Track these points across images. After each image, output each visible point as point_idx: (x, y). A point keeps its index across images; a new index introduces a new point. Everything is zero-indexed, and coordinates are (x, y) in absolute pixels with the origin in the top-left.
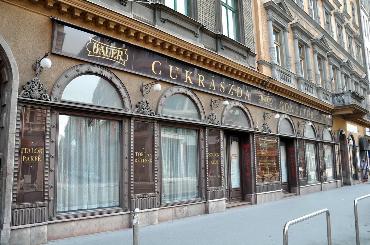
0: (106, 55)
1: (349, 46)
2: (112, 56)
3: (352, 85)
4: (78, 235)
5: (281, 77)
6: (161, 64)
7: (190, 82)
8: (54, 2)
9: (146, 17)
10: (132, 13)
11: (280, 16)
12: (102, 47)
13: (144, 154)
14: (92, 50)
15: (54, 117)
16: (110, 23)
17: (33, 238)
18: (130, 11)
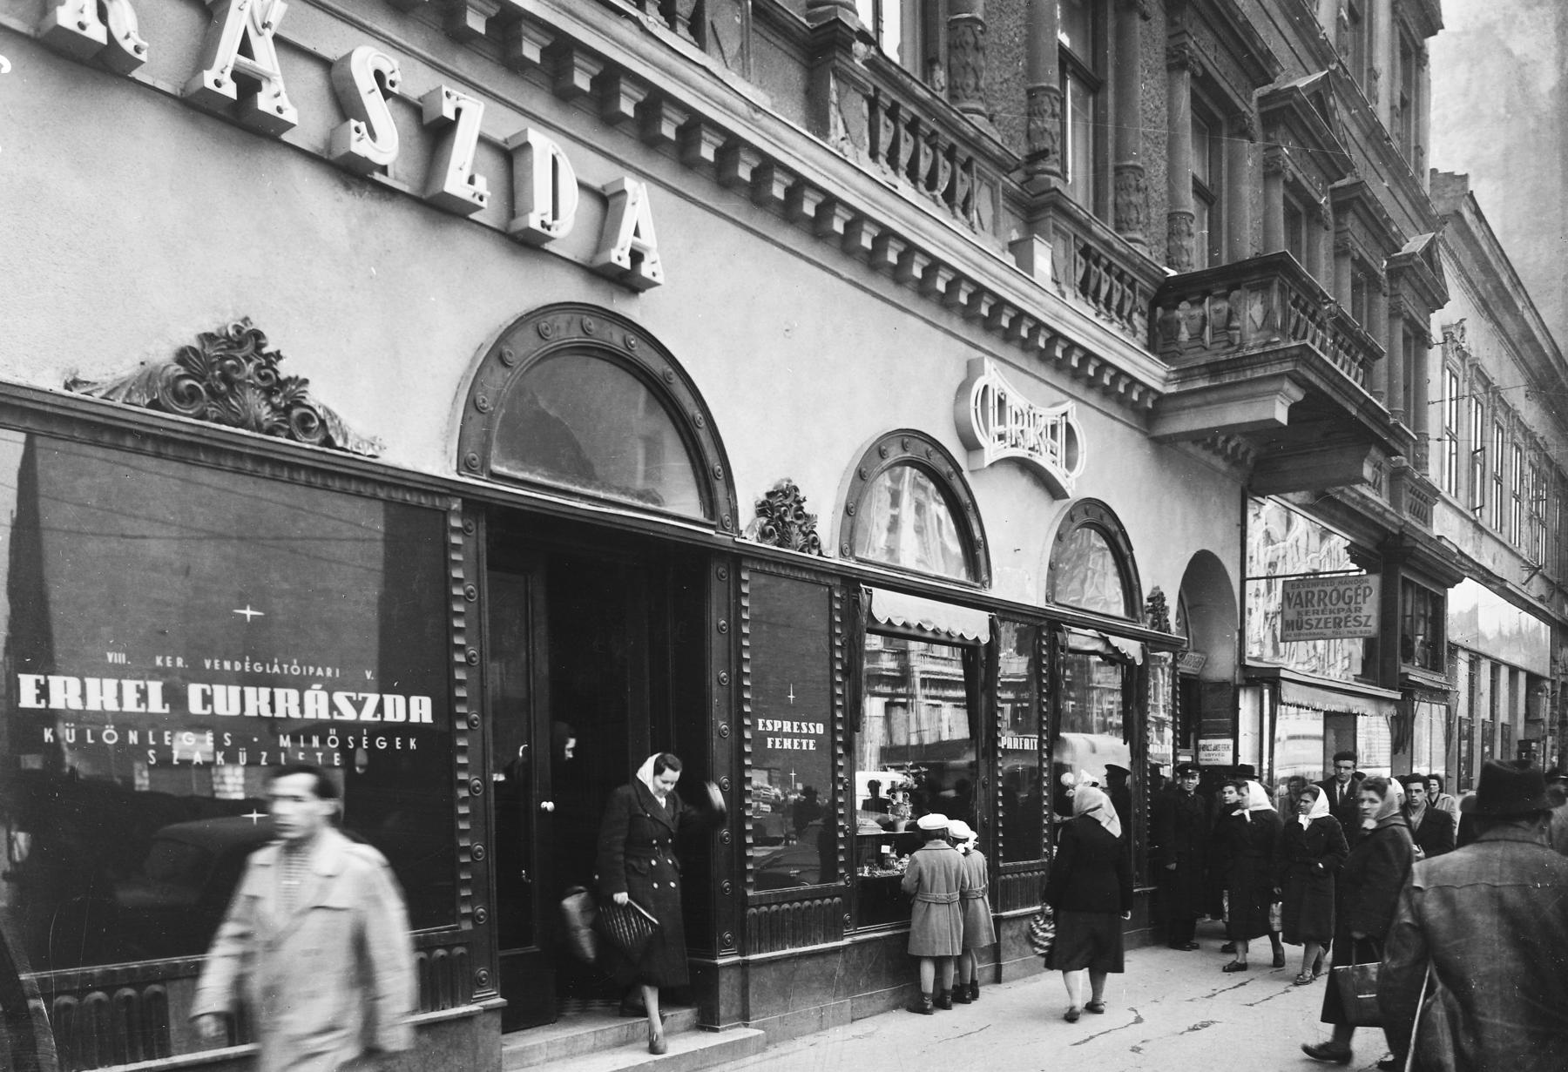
1: (1398, 103)
3: (1391, 330)
5: (884, 147)
8: (493, 11)
11: (1227, 48)
16: (623, 87)
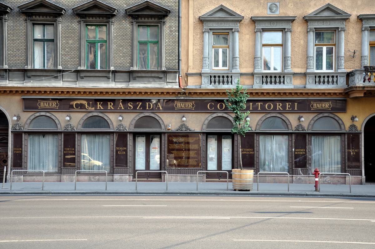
0: (184, 107)
2: (187, 107)
4: (36, 182)
6: (213, 104)
7: (122, 108)
9: (72, 79)
10: (62, 80)
12: (45, 103)
13: (69, 149)
14: (40, 106)
15: (79, 136)
17: (17, 180)
18: (61, 80)
